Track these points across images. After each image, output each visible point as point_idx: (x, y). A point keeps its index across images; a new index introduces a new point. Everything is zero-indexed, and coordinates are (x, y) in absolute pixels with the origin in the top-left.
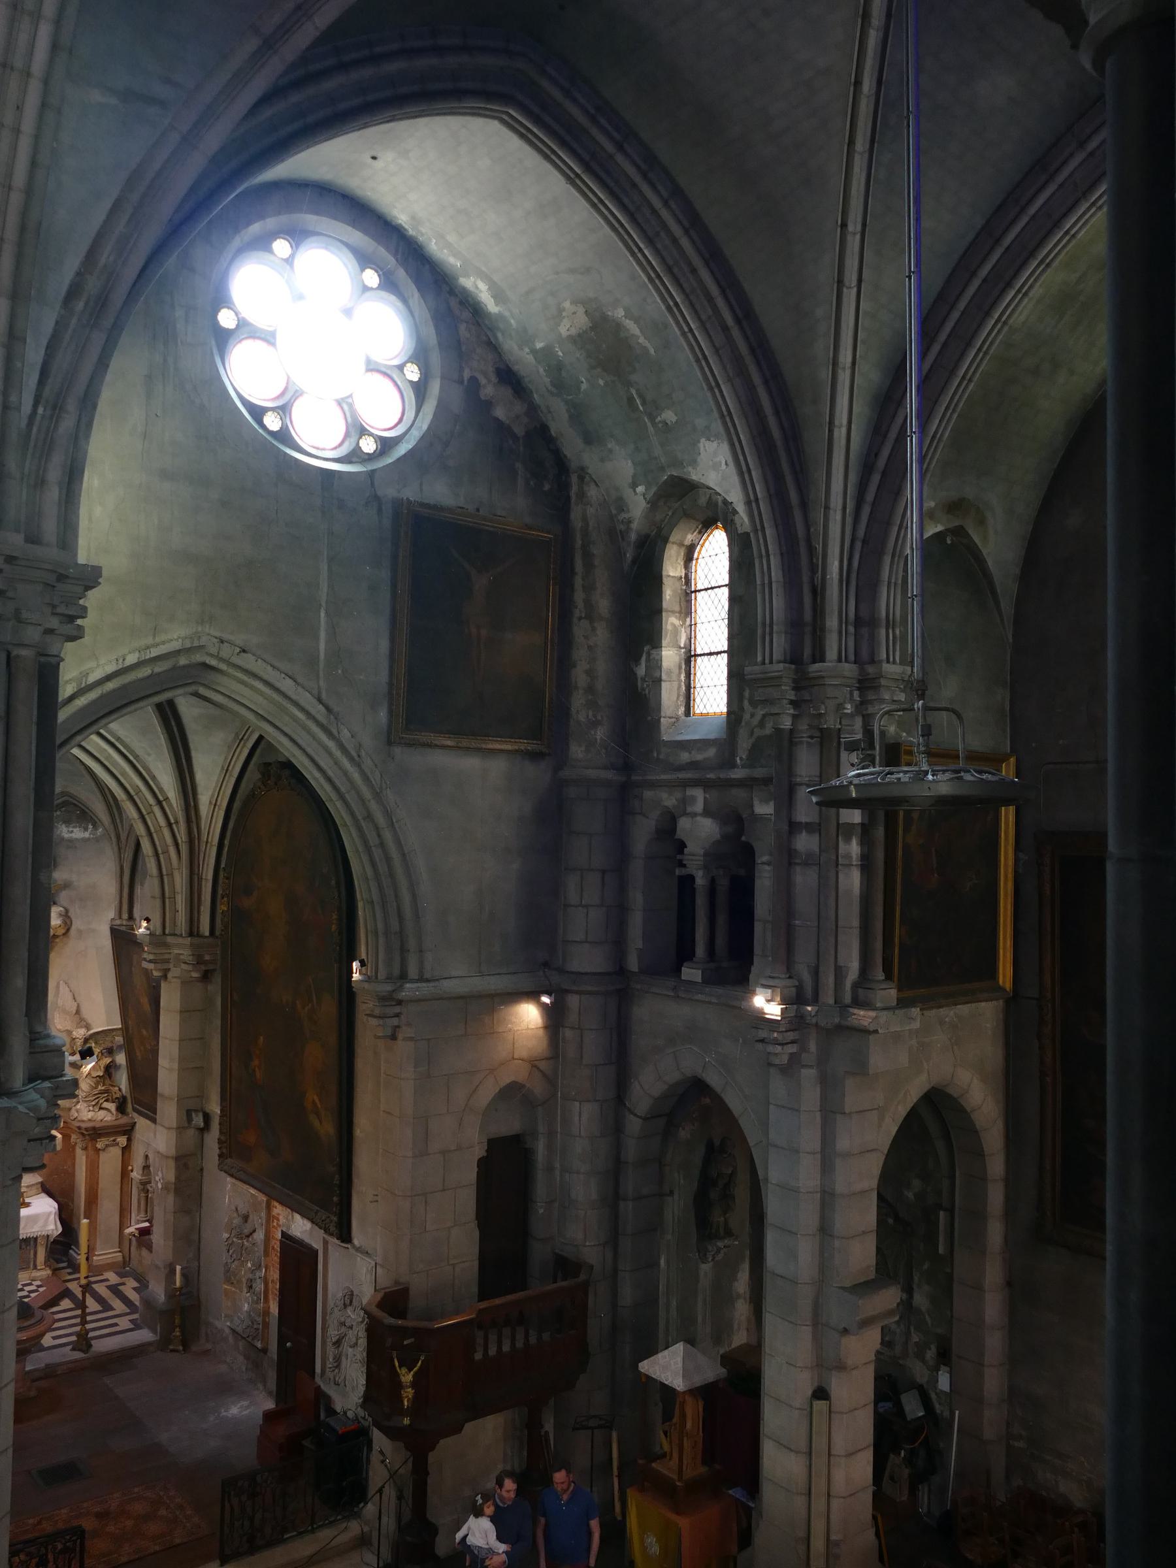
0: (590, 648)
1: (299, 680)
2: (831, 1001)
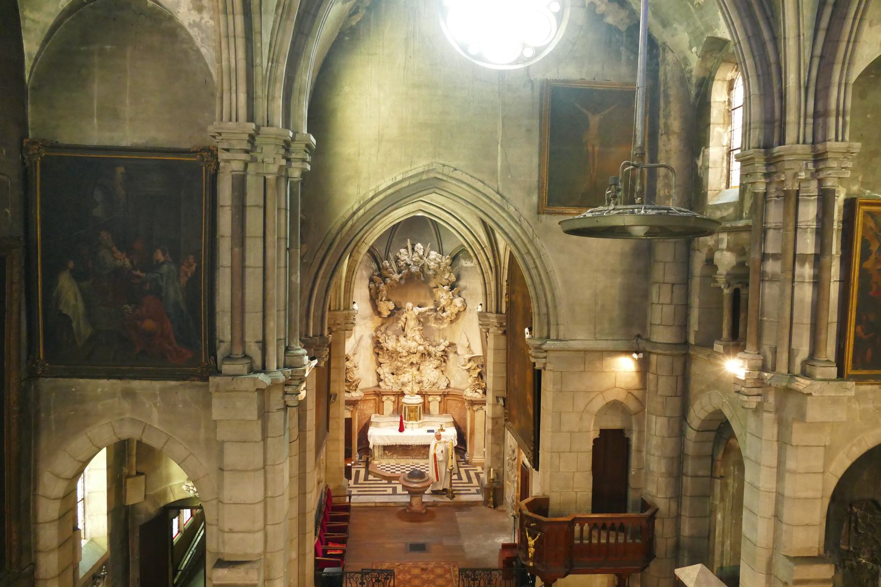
0: (666, 151)
1: (486, 182)
2: (785, 371)
